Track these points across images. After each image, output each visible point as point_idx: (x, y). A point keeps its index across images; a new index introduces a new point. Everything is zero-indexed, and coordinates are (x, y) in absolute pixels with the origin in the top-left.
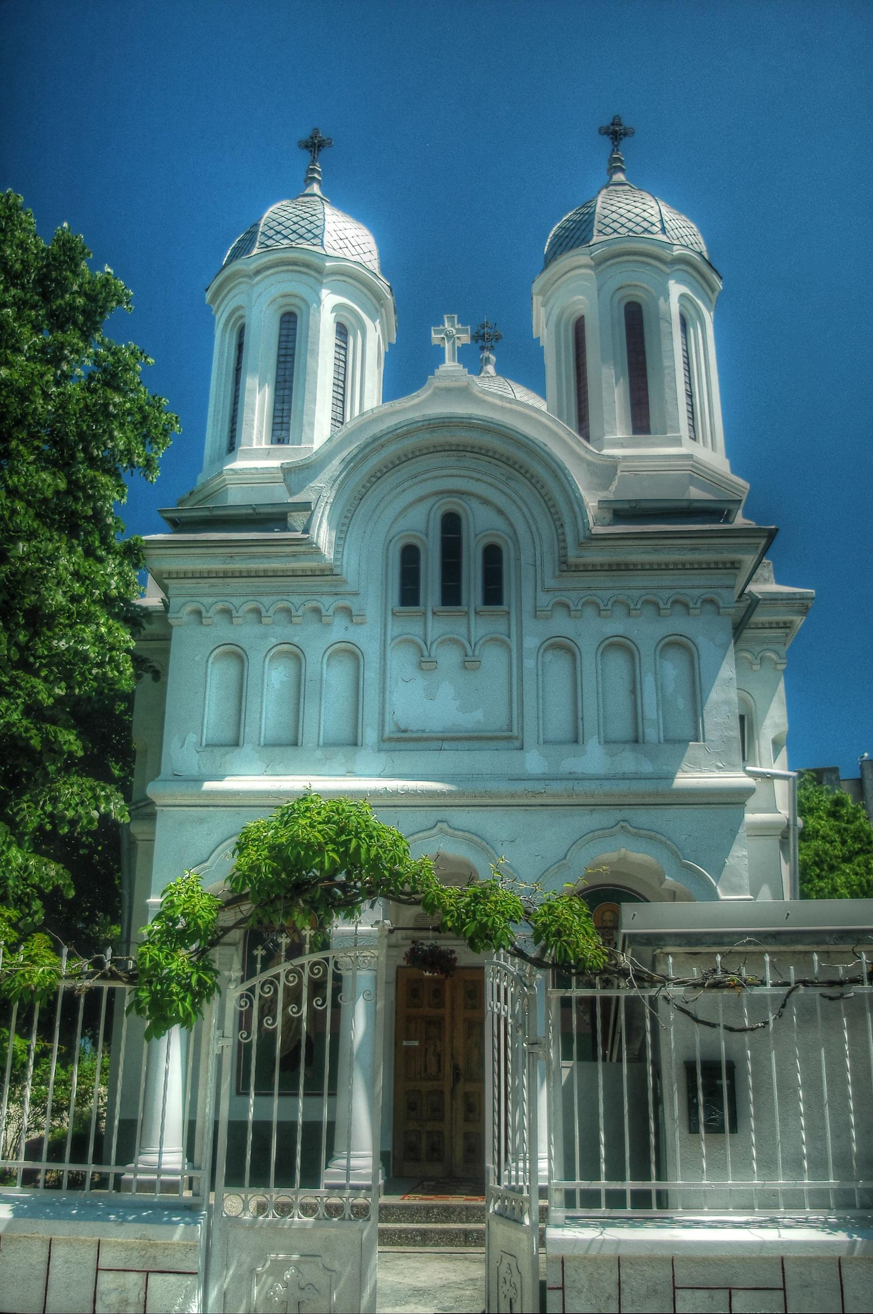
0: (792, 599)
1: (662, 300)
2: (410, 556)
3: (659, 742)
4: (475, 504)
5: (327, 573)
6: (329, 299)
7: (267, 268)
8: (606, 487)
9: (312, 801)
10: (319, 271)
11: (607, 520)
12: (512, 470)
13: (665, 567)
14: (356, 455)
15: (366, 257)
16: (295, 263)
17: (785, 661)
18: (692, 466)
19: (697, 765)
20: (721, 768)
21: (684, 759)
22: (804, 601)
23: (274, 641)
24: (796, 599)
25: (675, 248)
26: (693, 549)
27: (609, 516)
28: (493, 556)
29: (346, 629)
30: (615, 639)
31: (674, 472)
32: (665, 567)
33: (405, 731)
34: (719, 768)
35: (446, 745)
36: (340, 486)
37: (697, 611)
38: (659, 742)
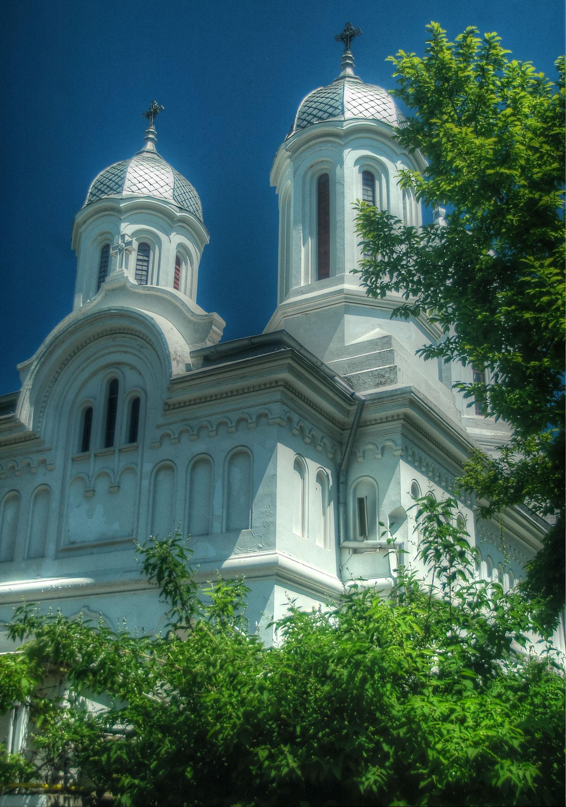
0: (393, 396)
1: (339, 167)
2: (88, 414)
3: (222, 532)
4: (127, 370)
5: (31, 438)
6: (128, 229)
7: (92, 216)
8: (203, 340)
9: (402, 637)
10: (119, 211)
11: (200, 365)
12: (144, 342)
13: (232, 394)
14: (45, 352)
15: (391, 119)
16: (105, 210)
17: (400, 447)
18: (345, 298)
19: (245, 548)
20: (261, 548)
21: (237, 544)
22: (404, 396)
23: (6, 489)
24: (398, 395)
25: (345, 124)
26: (243, 377)
27: (201, 362)
28: (136, 404)
29: (45, 475)
30: (201, 456)
31: (340, 305)
32: (232, 394)
33: (73, 543)
34: (260, 548)
35: (95, 550)
36: (36, 376)
37: (254, 425)
38: (222, 532)
